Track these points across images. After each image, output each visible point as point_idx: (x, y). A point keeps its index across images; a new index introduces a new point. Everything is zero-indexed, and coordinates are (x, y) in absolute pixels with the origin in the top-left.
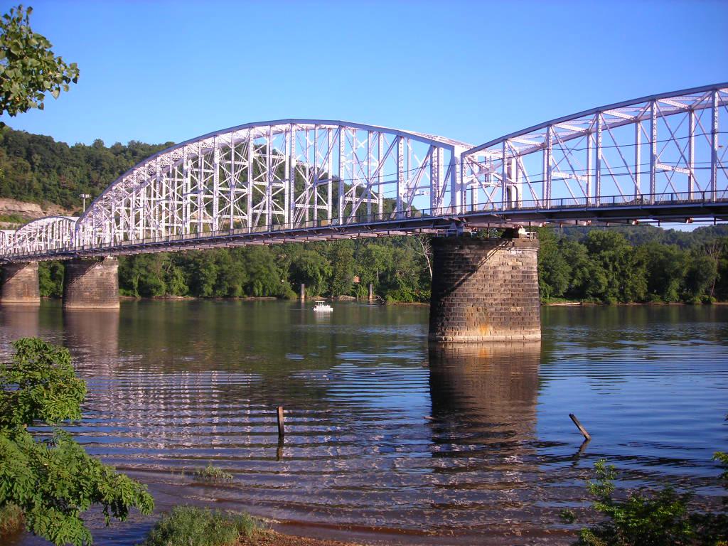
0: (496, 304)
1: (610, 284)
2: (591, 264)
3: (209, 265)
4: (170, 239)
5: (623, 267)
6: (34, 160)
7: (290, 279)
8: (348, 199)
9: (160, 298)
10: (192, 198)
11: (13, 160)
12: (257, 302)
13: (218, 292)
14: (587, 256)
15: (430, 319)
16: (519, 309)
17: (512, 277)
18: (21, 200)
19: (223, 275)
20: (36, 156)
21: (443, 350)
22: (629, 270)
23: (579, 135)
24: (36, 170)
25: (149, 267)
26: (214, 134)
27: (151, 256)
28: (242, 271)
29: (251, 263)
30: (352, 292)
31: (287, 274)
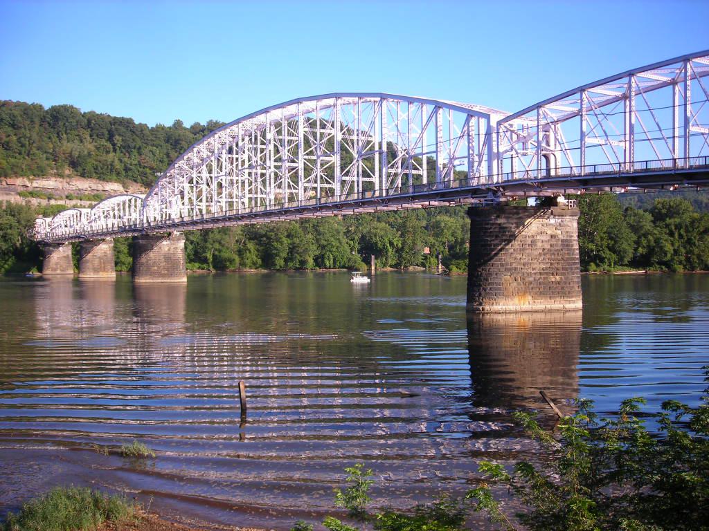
0: (535, 274)
1: (676, 252)
2: (655, 232)
3: (281, 238)
4: (254, 211)
5: (689, 234)
6: (116, 142)
7: (359, 252)
8: (393, 171)
9: (234, 271)
10: (275, 167)
11: (96, 142)
12: (328, 274)
13: (290, 264)
14: (652, 224)
15: (468, 289)
16: (558, 278)
17: (551, 246)
18: (104, 180)
19: (294, 247)
20: (117, 137)
21: (480, 321)
22: (695, 237)
23: (616, 99)
24: (118, 151)
25: (222, 242)
26: (266, 111)
27: (224, 231)
28: (313, 244)
29: (321, 237)
30: (422, 263)
31: (357, 246)
